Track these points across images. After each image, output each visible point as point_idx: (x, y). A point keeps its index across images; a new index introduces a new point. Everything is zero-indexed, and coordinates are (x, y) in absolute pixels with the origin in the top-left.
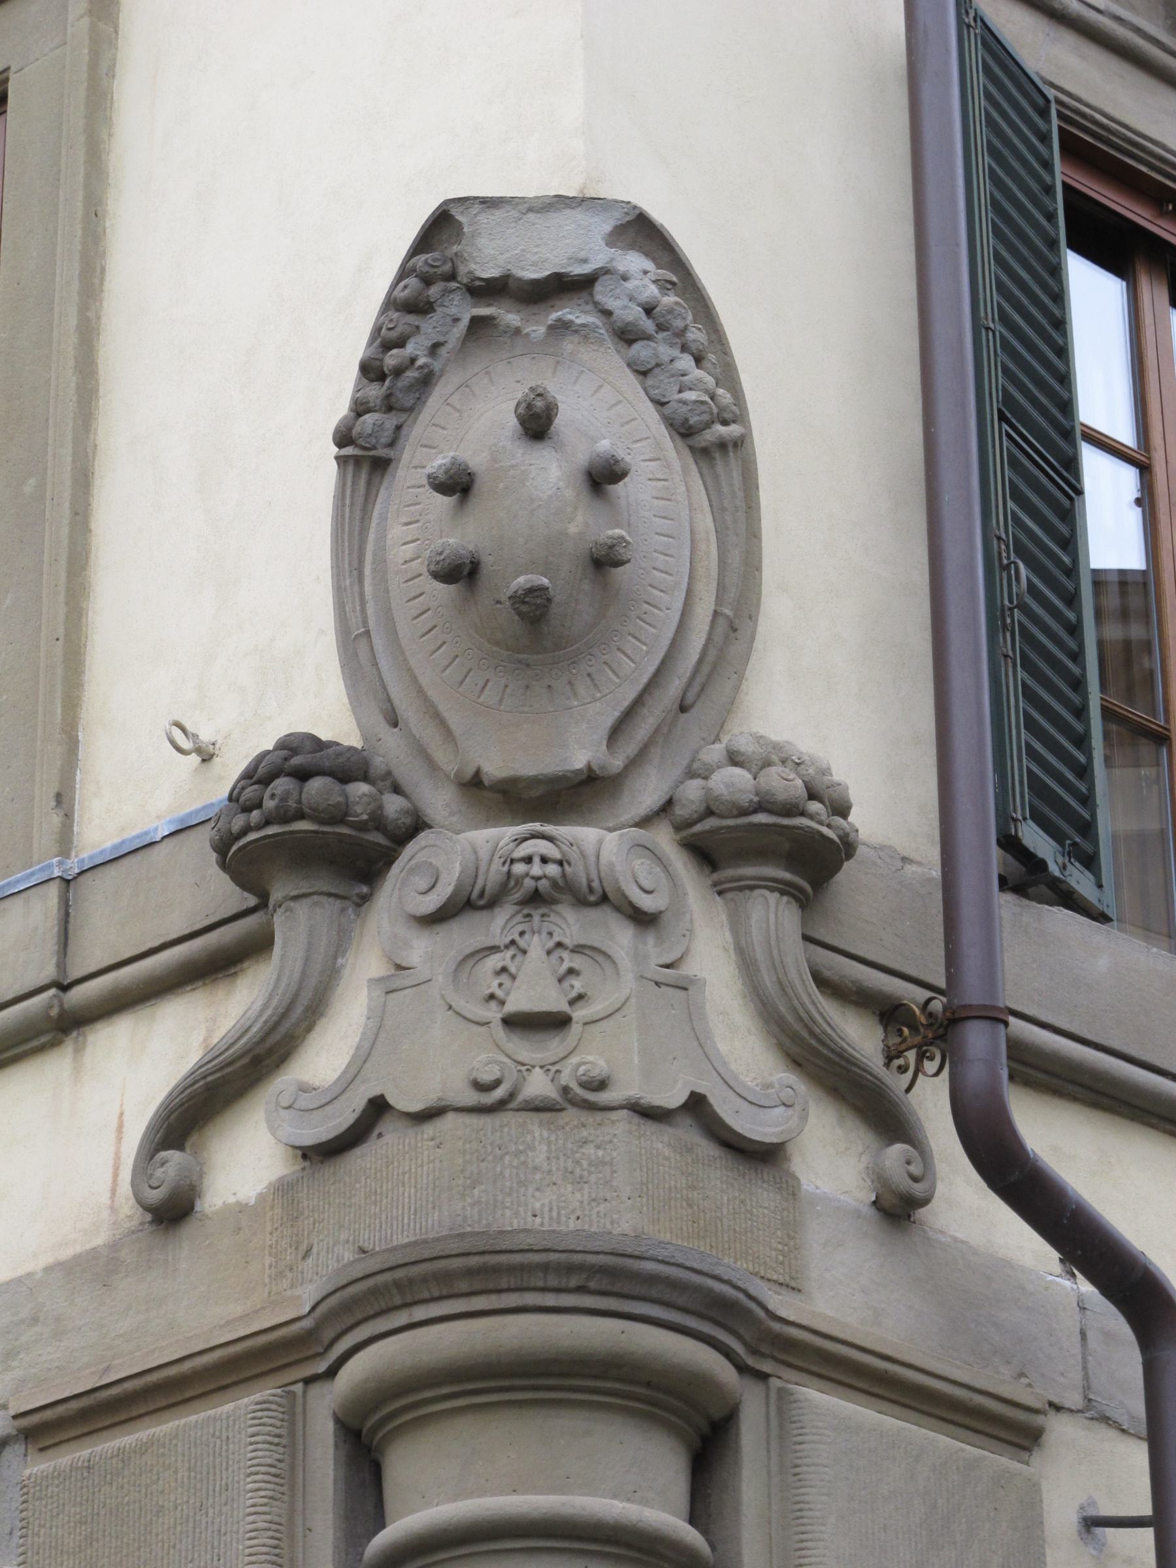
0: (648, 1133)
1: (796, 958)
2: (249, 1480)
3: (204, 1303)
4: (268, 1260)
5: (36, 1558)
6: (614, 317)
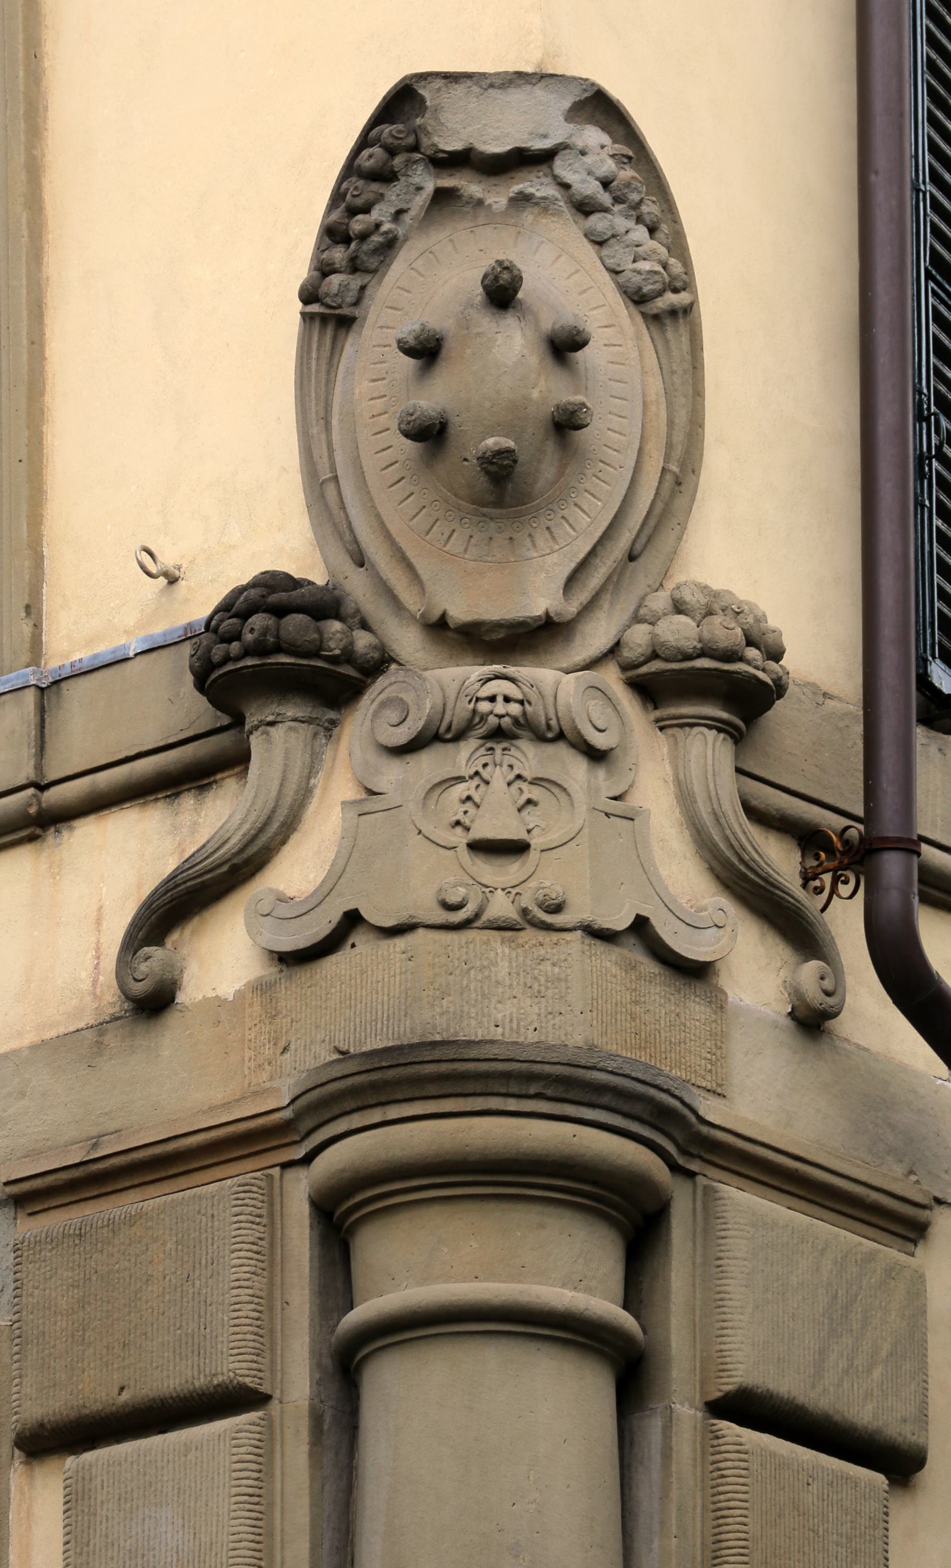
0: (598, 953)
1: (728, 788)
2: (234, 1255)
3: (184, 1083)
4: (248, 1054)
5: (31, 1317)
6: (573, 190)
